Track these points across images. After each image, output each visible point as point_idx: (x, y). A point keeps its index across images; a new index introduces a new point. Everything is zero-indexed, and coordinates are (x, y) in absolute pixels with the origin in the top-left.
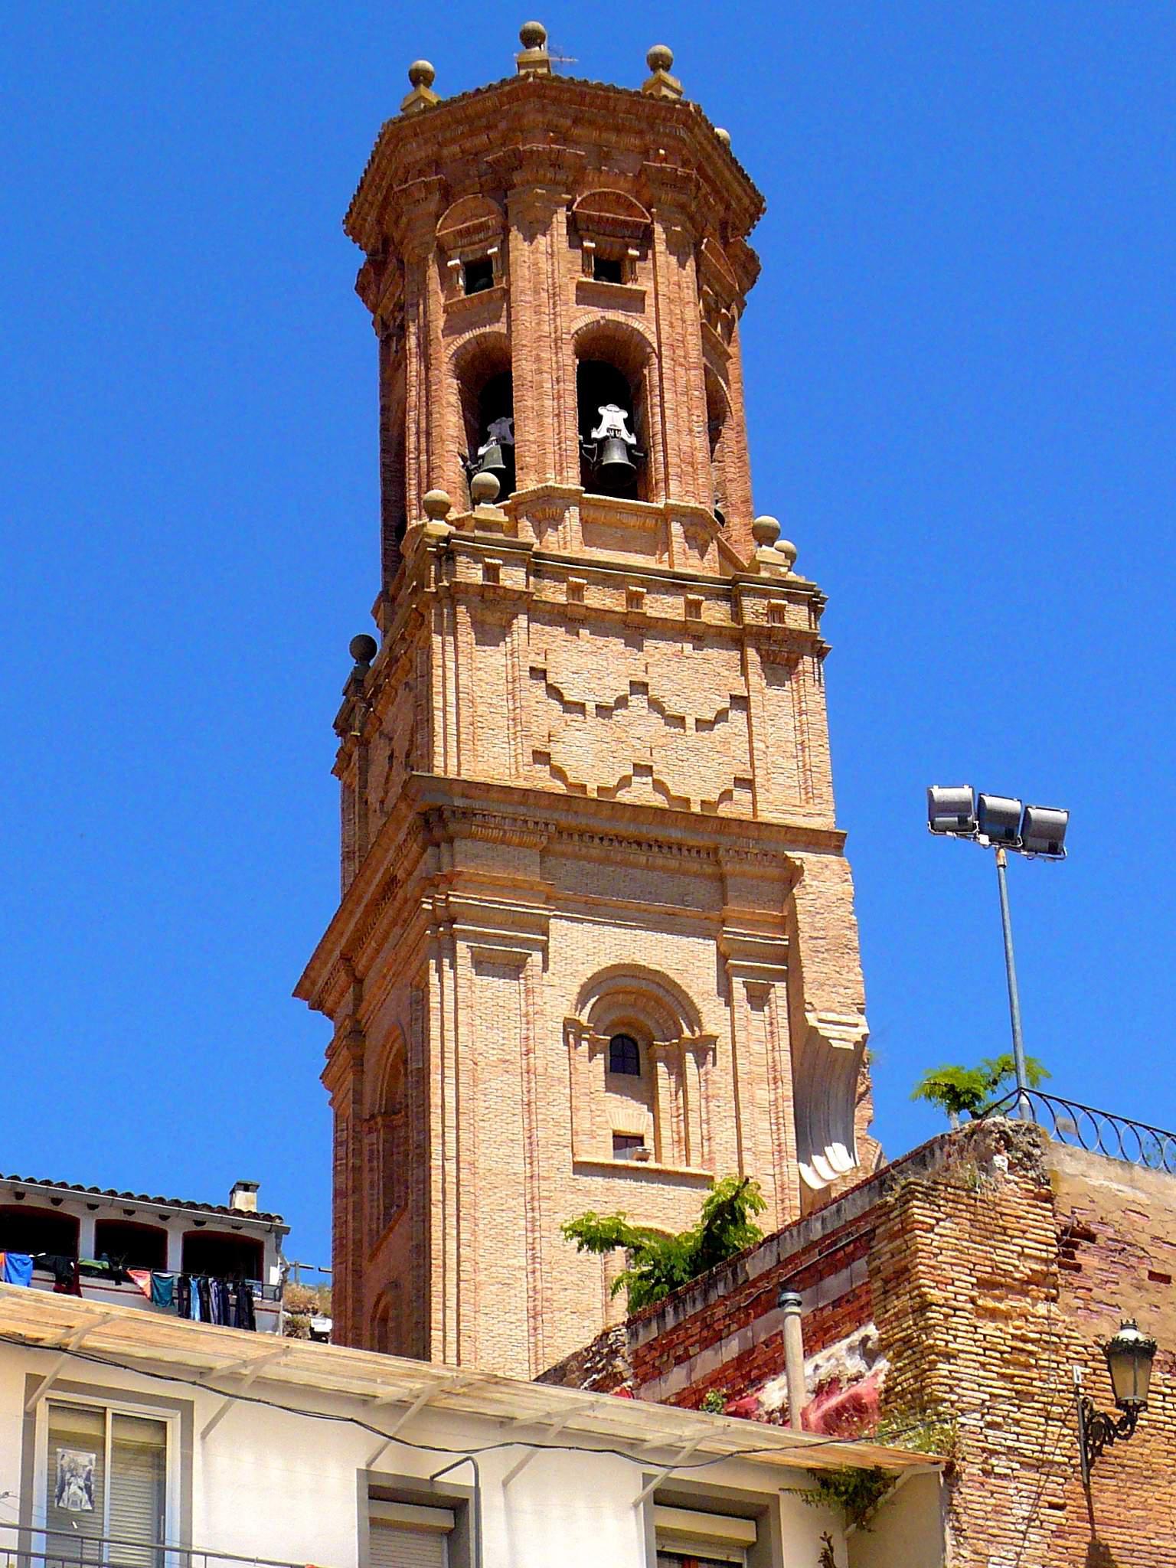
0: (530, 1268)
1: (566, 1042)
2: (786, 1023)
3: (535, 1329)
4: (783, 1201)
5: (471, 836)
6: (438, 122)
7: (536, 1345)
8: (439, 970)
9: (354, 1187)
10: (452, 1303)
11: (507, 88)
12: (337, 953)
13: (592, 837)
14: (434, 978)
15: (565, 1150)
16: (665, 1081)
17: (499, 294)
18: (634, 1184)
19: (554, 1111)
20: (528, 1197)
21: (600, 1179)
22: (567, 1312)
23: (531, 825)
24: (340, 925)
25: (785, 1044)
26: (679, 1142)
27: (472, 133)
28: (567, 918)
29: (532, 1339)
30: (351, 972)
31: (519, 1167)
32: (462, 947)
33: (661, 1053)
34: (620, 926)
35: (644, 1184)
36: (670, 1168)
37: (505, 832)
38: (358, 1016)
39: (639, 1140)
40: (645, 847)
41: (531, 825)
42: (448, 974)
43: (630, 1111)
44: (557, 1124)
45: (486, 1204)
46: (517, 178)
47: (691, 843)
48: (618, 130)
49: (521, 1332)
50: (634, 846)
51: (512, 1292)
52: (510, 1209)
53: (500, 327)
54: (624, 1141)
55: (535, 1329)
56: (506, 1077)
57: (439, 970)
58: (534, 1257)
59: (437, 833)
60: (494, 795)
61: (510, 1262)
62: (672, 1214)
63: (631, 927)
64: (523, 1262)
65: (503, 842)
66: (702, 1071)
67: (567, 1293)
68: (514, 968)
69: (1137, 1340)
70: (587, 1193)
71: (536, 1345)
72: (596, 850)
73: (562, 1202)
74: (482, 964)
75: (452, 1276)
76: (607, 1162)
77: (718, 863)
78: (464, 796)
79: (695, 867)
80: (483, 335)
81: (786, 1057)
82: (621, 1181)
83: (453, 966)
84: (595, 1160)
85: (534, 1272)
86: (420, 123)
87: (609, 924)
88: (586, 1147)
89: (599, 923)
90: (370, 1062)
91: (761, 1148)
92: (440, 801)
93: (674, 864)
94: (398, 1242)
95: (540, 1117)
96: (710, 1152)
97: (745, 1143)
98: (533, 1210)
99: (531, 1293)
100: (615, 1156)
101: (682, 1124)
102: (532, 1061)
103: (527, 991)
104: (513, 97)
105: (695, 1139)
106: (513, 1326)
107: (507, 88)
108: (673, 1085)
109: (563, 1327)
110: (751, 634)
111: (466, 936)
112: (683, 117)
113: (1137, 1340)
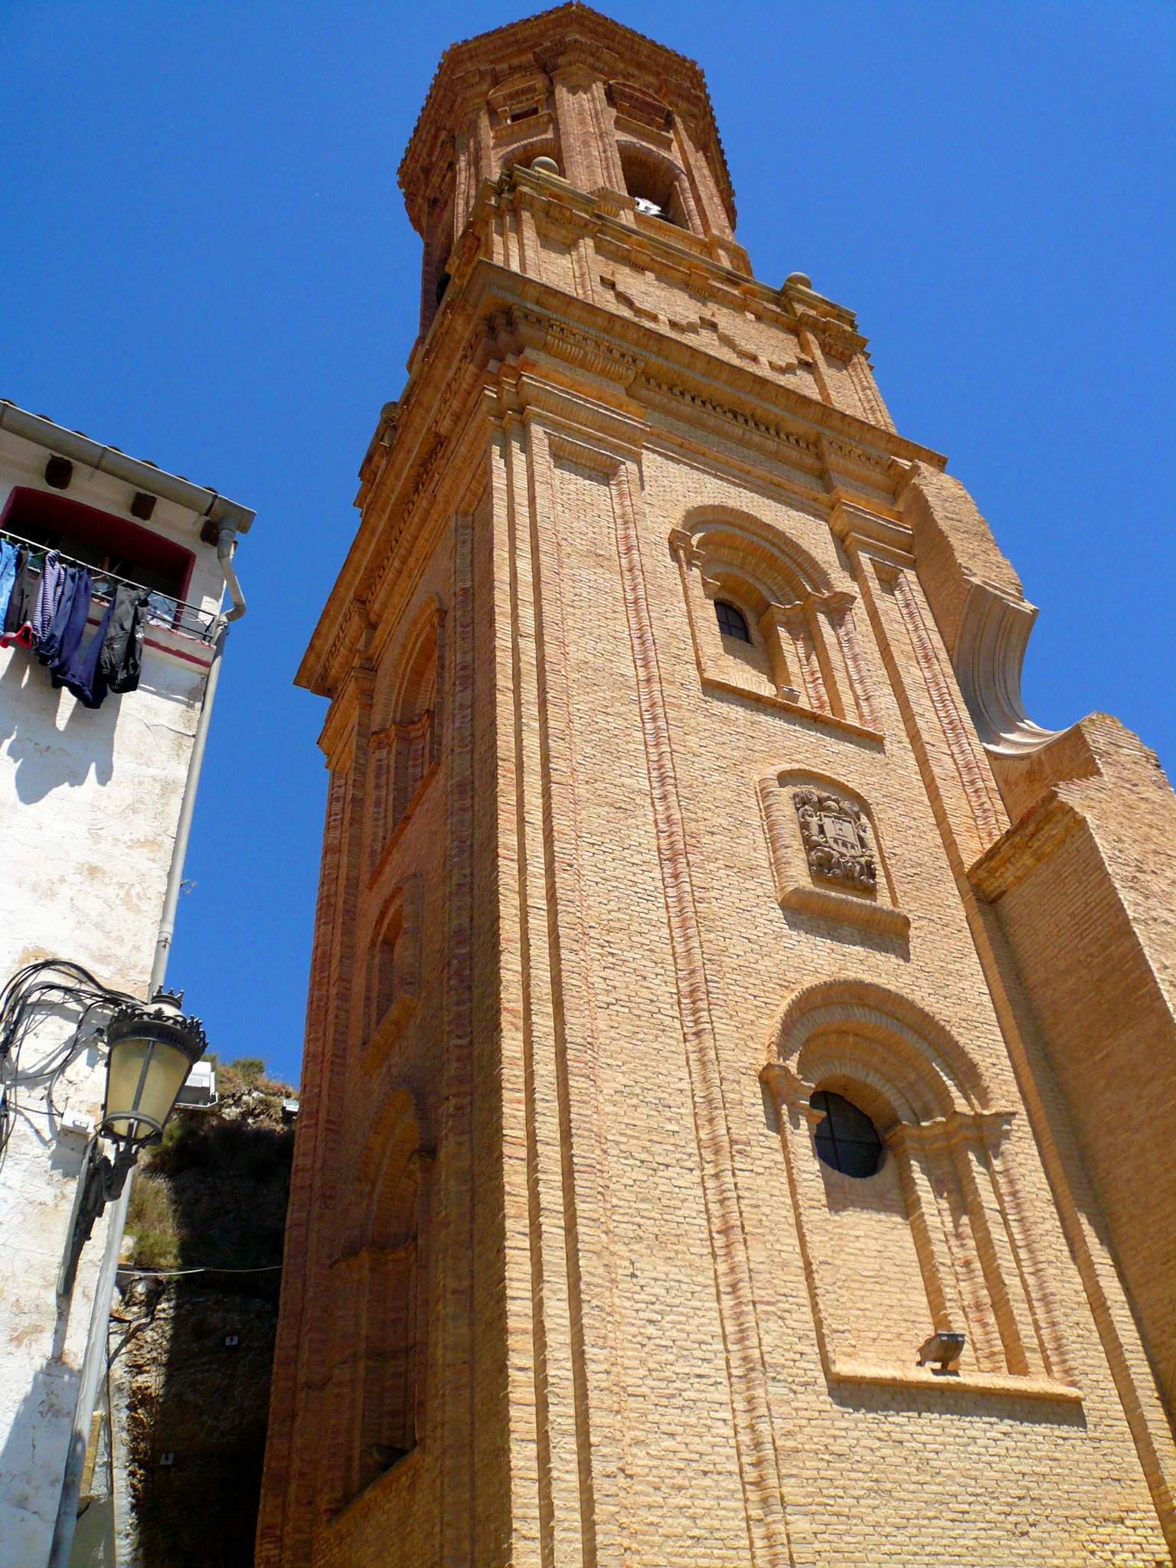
0: (657, 793)
1: (675, 557)
2: (926, 606)
3: (676, 876)
4: (972, 782)
5: (545, 348)
6: (491, 47)
7: (680, 900)
8: (506, 455)
9: (352, 819)
10: (535, 816)
11: (553, 16)
12: (351, 594)
13: (682, 394)
14: (498, 463)
16: (791, 649)
17: (546, 119)
20: (645, 705)
23: (616, 354)
24: (357, 555)
25: (930, 623)
27: (521, 52)
28: (660, 454)
29: (671, 892)
30: (365, 615)
32: (537, 431)
33: (778, 617)
34: (722, 479)
37: (586, 353)
38: (370, 652)
40: (741, 419)
41: (616, 354)
42: (519, 460)
45: (581, 703)
46: (561, 60)
47: (791, 428)
48: (639, 66)
49: (653, 878)
50: (730, 415)
51: (631, 821)
52: (620, 715)
53: (550, 135)
55: (676, 876)
56: (600, 571)
57: (506, 455)
59: (504, 337)
60: (576, 312)
61: (627, 781)
63: (734, 484)
65: (582, 365)
66: (842, 631)
68: (605, 474)
70: (725, 720)
71: (680, 900)
72: (686, 408)
74: (561, 457)
75: (533, 782)
77: (820, 457)
78: (538, 302)
79: (794, 454)
80: (531, 144)
81: (936, 637)
83: (526, 449)
86: (475, 48)
87: (709, 474)
89: (697, 469)
90: (379, 699)
92: (510, 299)
93: (771, 445)
94: (425, 836)
96: (872, 712)
98: (654, 719)
99: (662, 826)
102: (636, 557)
103: (621, 495)
104: (558, 23)
106: (635, 869)
107: (553, 16)
108: (801, 651)
110: (806, 324)
111: (543, 421)
112: (690, 74)
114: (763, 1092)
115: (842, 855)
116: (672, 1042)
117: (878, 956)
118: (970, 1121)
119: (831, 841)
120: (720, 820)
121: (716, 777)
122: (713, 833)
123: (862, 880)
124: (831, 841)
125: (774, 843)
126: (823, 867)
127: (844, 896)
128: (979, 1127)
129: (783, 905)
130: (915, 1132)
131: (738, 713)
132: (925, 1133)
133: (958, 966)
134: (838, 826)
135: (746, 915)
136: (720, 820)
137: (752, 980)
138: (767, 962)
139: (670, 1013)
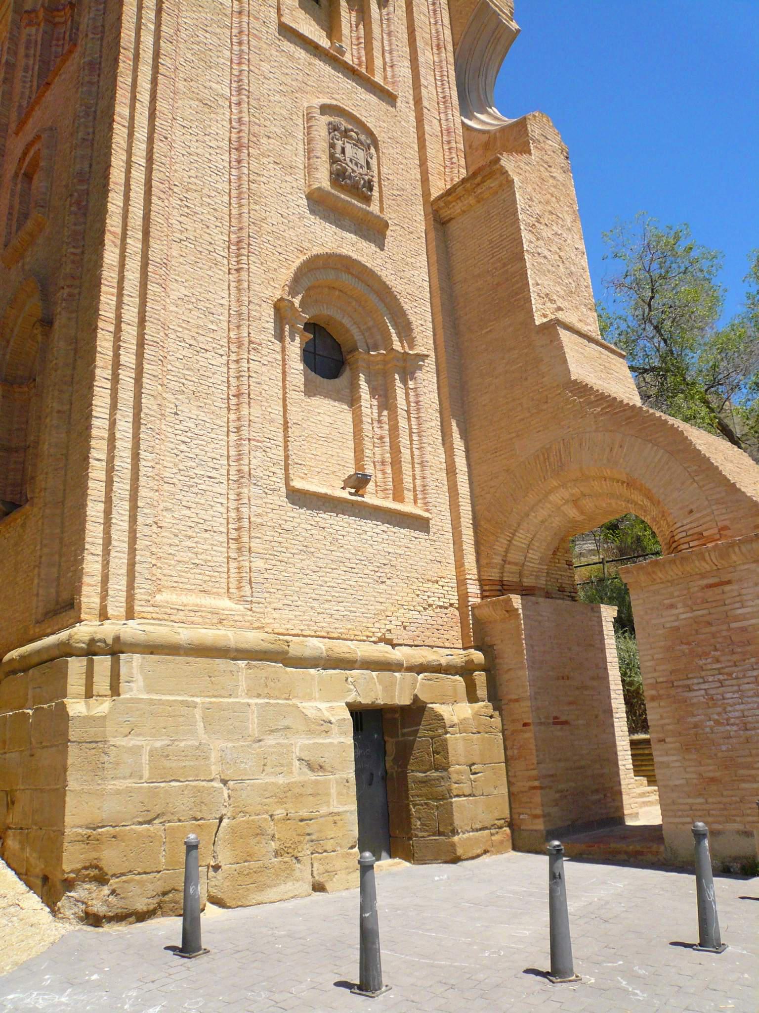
22: (271, 159)
70: (291, 57)
115: (353, 171)
116: (220, 272)
118: (401, 356)
123: (362, 190)
125: (309, 153)
128: (405, 360)
129: (309, 197)
130: (366, 357)
134: (355, 151)
135: (283, 198)
137: (279, 242)
138: (291, 232)
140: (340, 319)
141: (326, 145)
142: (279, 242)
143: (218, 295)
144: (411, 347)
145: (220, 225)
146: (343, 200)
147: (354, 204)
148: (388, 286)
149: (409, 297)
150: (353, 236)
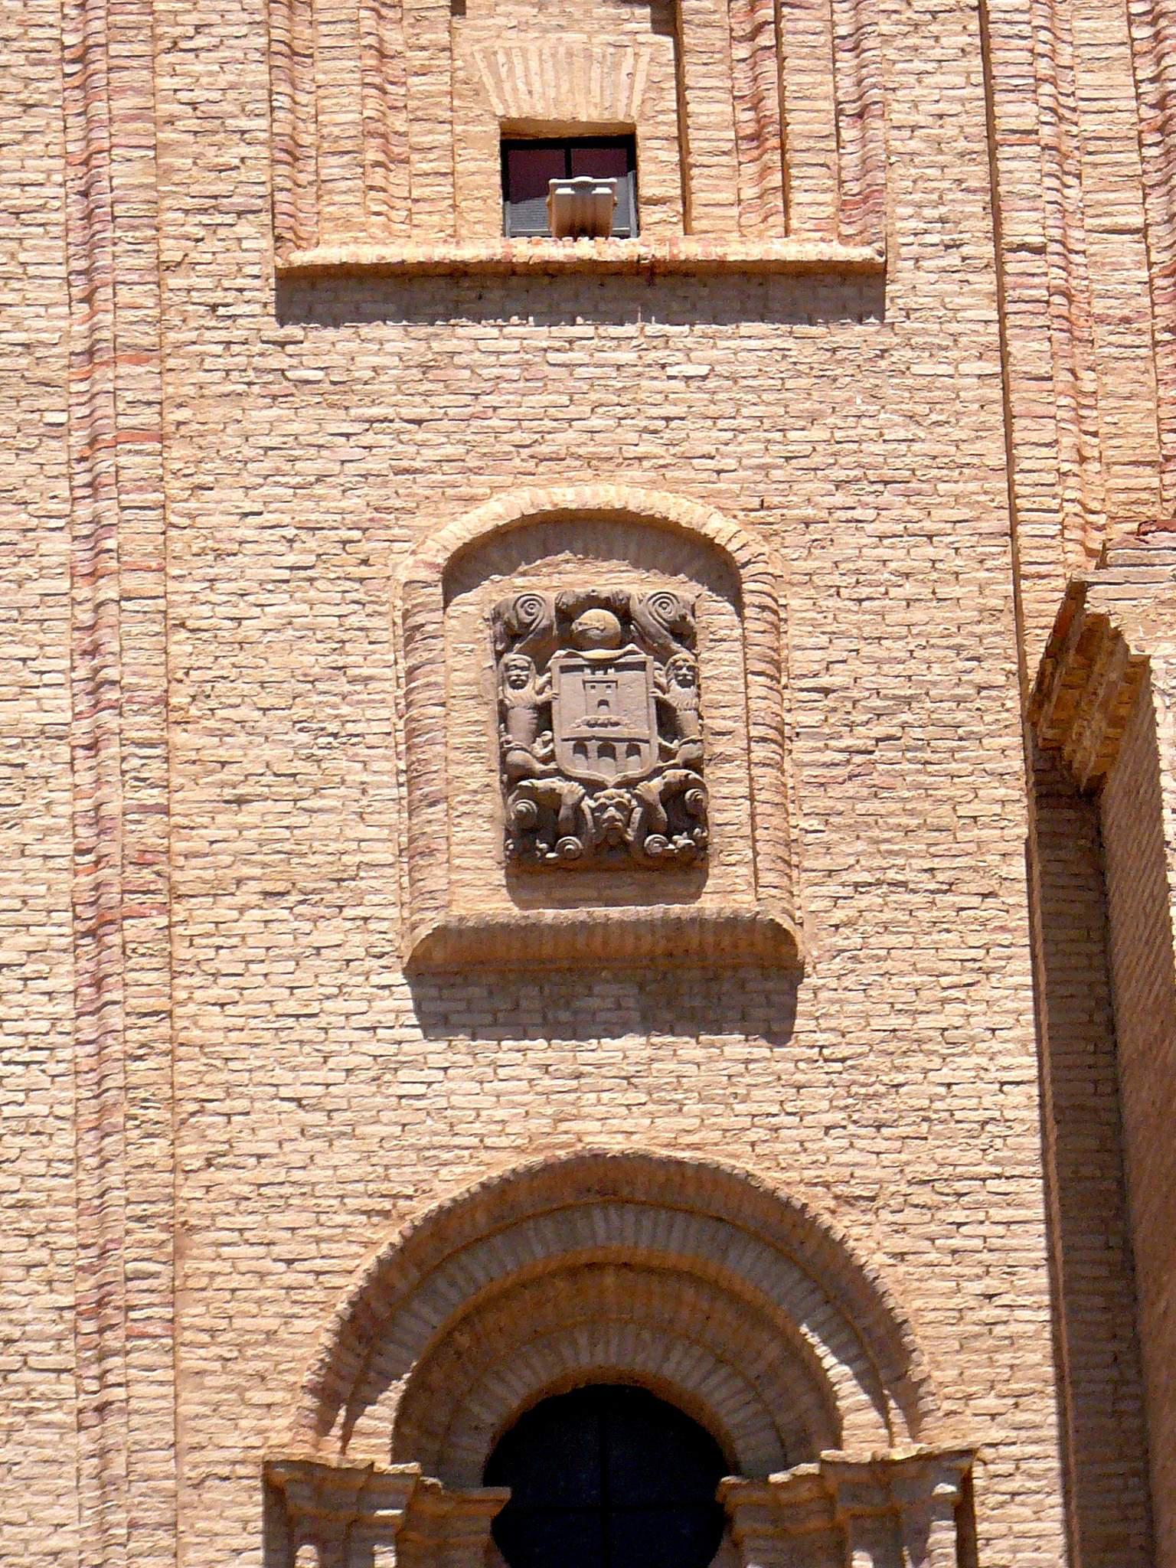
15: (244, 228)
18: (538, 335)
19: (200, 75)
21: (390, 332)
22: (248, 894)
26: (757, 137)
31: (51, 320)
35: (582, 329)
36: (737, 251)
39: (616, 149)
43: (575, 38)
44: (210, 123)
54: (532, 159)
58: (97, 685)
62: (702, 439)
64: (59, 706)
67: (247, 816)
69: (380, 1260)
70: (339, 390)
73: (231, 438)
76: (470, 252)
82: (485, 330)
84: (368, 254)
85: (93, 747)
88: (343, 200)
91: (1090, 124)
95: (124, 104)
97: (1015, 113)
100: (508, 232)
101: (770, 65)
105: (808, 121)
109: (225, 961)
113: (380, 1260)
114: (267, 1515)
115: (593, 786)
116: (47, 1435)
117: (689, 1048)
118: (865, 1476)
119: (564, 750)
120: (268, 752)
121: (283, 605)
122: (240, 801)
123: (671, 834)
124: (564, 750)
125: (416, 787)
126: (541, 840)
127: (580, 914)
128: (886, 1488)
129: (418, 971)
130: (757, 1495)
131: (385, 344)
132: (784, 1496)
133: (952, 1015)
134: (597, 694)
135: (305, 1030)
136: (268, 752)
137: (289, 1218)
138: (343, 1154)
139: (52, 1361)
140: (651, 1366)
141: (486, 714)
142: (289, 1218)
143: (38, 1522)
144: (914, 1423)
145: (43, 1255)
146: (554, 929)
147: (606, 924)
148: (787, 1204)
149: (923, 1195)
150: (632, 1042)
